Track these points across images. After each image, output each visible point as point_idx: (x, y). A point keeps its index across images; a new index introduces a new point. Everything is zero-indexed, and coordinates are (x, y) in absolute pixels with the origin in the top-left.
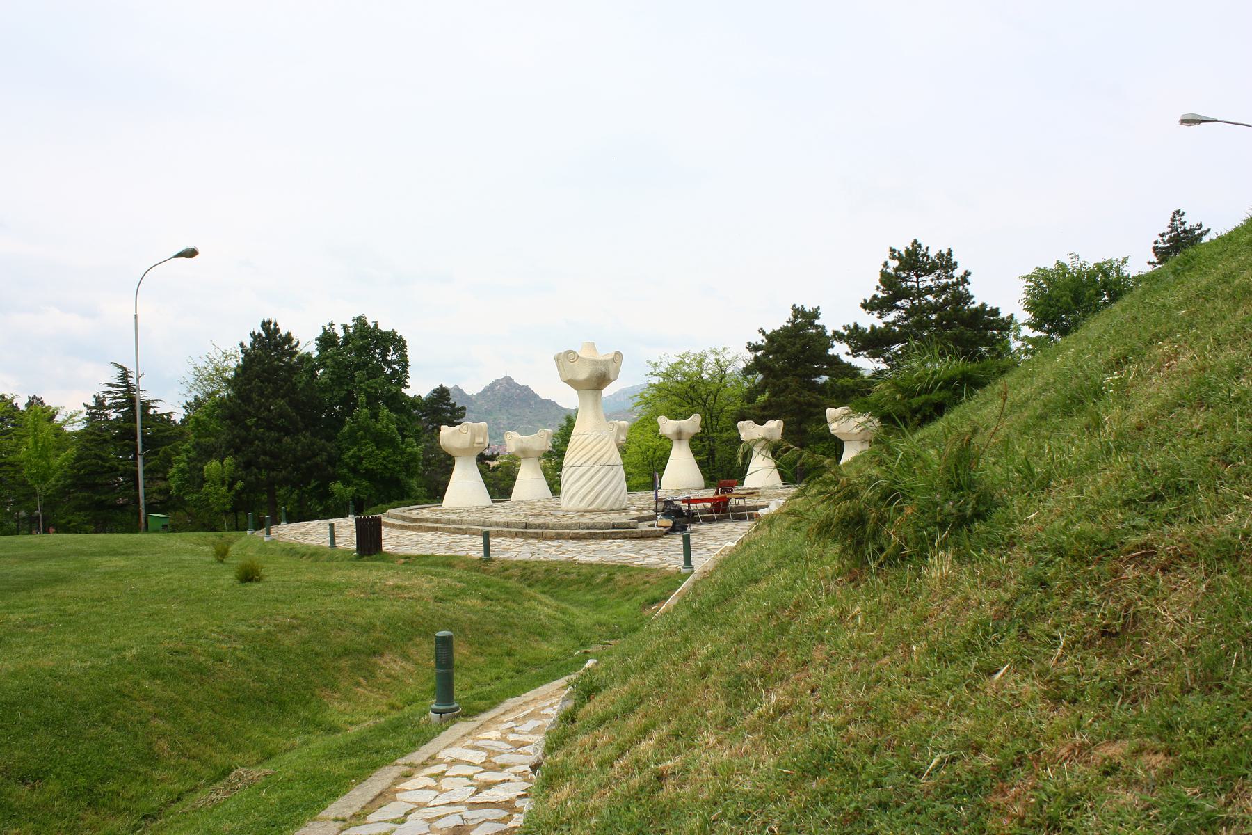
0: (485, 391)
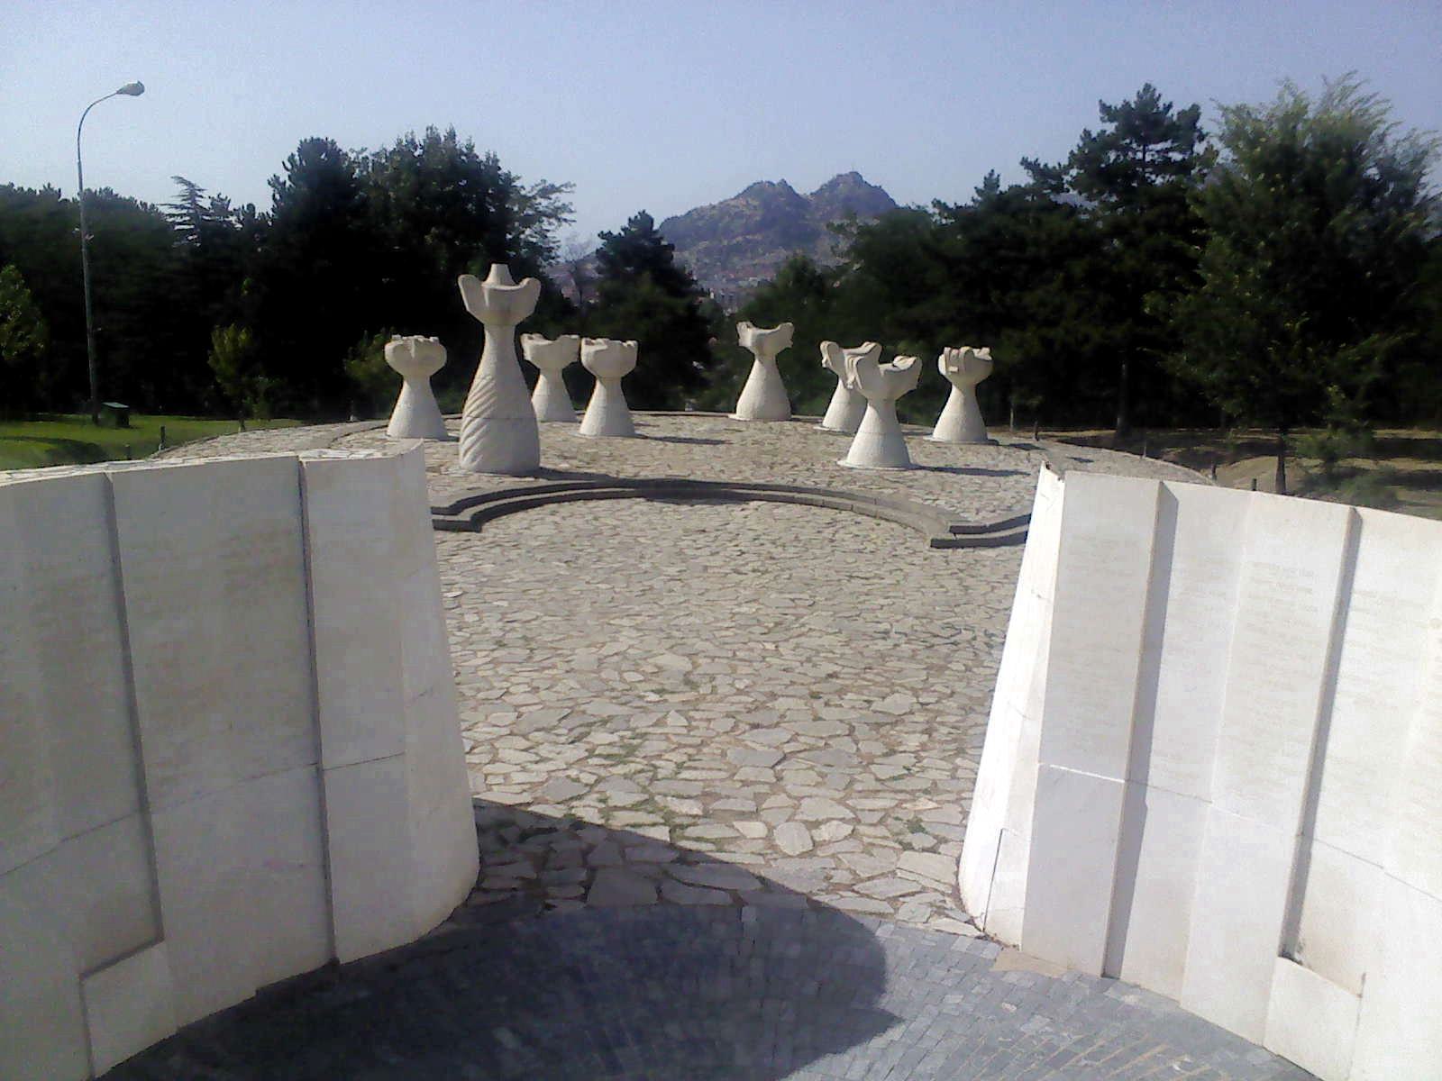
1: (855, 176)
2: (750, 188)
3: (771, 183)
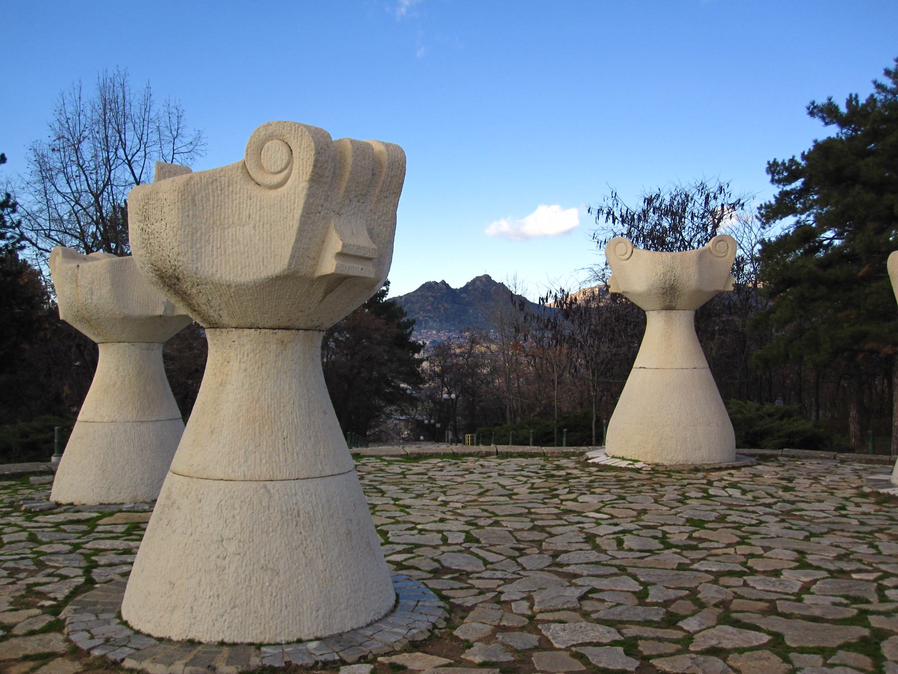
0: (468, 285)
1: (487, 277)
2: (423, 286)
3: (435, 283)
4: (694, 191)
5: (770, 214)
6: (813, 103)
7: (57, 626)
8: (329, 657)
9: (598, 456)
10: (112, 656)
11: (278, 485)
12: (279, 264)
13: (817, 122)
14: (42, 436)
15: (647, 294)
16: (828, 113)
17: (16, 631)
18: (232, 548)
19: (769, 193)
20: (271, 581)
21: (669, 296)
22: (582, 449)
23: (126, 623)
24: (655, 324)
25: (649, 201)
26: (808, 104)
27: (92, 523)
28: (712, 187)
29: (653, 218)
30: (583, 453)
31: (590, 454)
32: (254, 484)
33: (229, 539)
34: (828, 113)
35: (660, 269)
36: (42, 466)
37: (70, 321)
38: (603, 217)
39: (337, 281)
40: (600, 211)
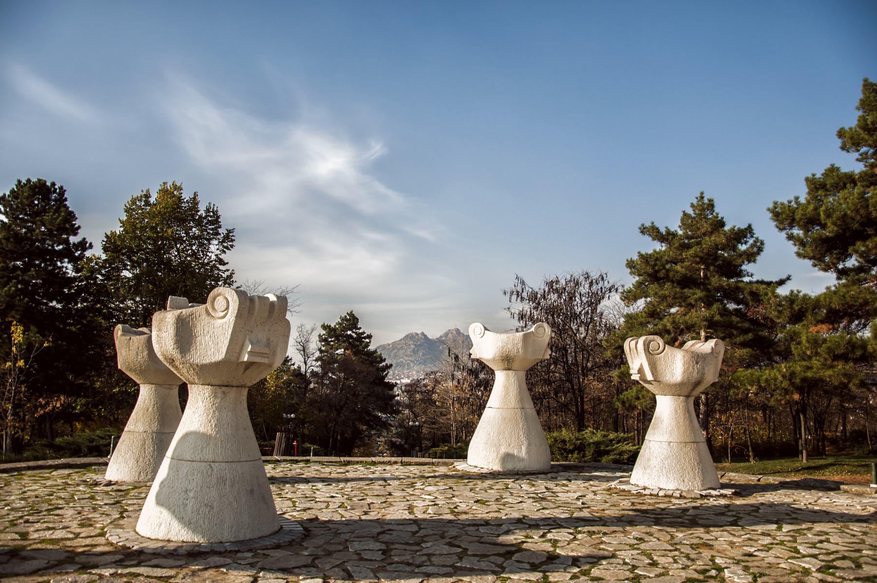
4: (582, 278)
5: (630, 297)
6: (643, 225)
7: (102, 534)
8: (233, 549)
9: (461, 466)
10: (128, 545)
11: (217, 464)
12: (220, 356)
13: (647, 238)
14: (102, 442)
15: (494, 360)
16: (653, 232)
17: (81, 535)
18: (191, 495)
19: (630, 281)
20: (209, 512)
21: (507, 361)
22: (451, 460)
23: (137, 533)
24: (501, 379)
25: (550, 284)
26: (640, 225)
27: (127, 492)
28: (594, 275)
29: (554, 297)
30: (452, 464)
31: (456, 464)
32: (205, 464)
33: (190, 490)
34: (653, 232)
35: (500, 344)
36: (101, 460)
37: (124, 370)
38: (514, 297)
39: (249, 365)
40: (512, 293)
